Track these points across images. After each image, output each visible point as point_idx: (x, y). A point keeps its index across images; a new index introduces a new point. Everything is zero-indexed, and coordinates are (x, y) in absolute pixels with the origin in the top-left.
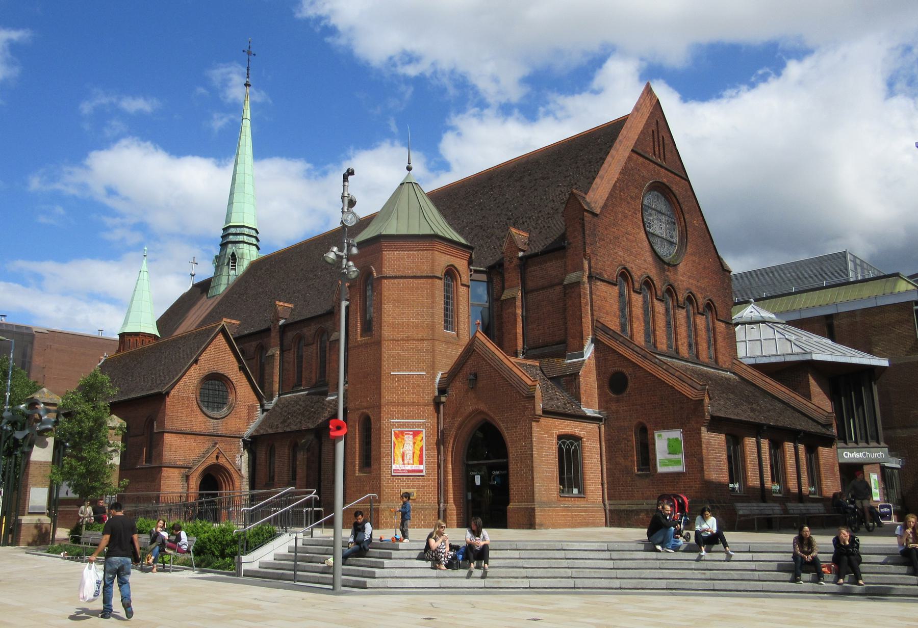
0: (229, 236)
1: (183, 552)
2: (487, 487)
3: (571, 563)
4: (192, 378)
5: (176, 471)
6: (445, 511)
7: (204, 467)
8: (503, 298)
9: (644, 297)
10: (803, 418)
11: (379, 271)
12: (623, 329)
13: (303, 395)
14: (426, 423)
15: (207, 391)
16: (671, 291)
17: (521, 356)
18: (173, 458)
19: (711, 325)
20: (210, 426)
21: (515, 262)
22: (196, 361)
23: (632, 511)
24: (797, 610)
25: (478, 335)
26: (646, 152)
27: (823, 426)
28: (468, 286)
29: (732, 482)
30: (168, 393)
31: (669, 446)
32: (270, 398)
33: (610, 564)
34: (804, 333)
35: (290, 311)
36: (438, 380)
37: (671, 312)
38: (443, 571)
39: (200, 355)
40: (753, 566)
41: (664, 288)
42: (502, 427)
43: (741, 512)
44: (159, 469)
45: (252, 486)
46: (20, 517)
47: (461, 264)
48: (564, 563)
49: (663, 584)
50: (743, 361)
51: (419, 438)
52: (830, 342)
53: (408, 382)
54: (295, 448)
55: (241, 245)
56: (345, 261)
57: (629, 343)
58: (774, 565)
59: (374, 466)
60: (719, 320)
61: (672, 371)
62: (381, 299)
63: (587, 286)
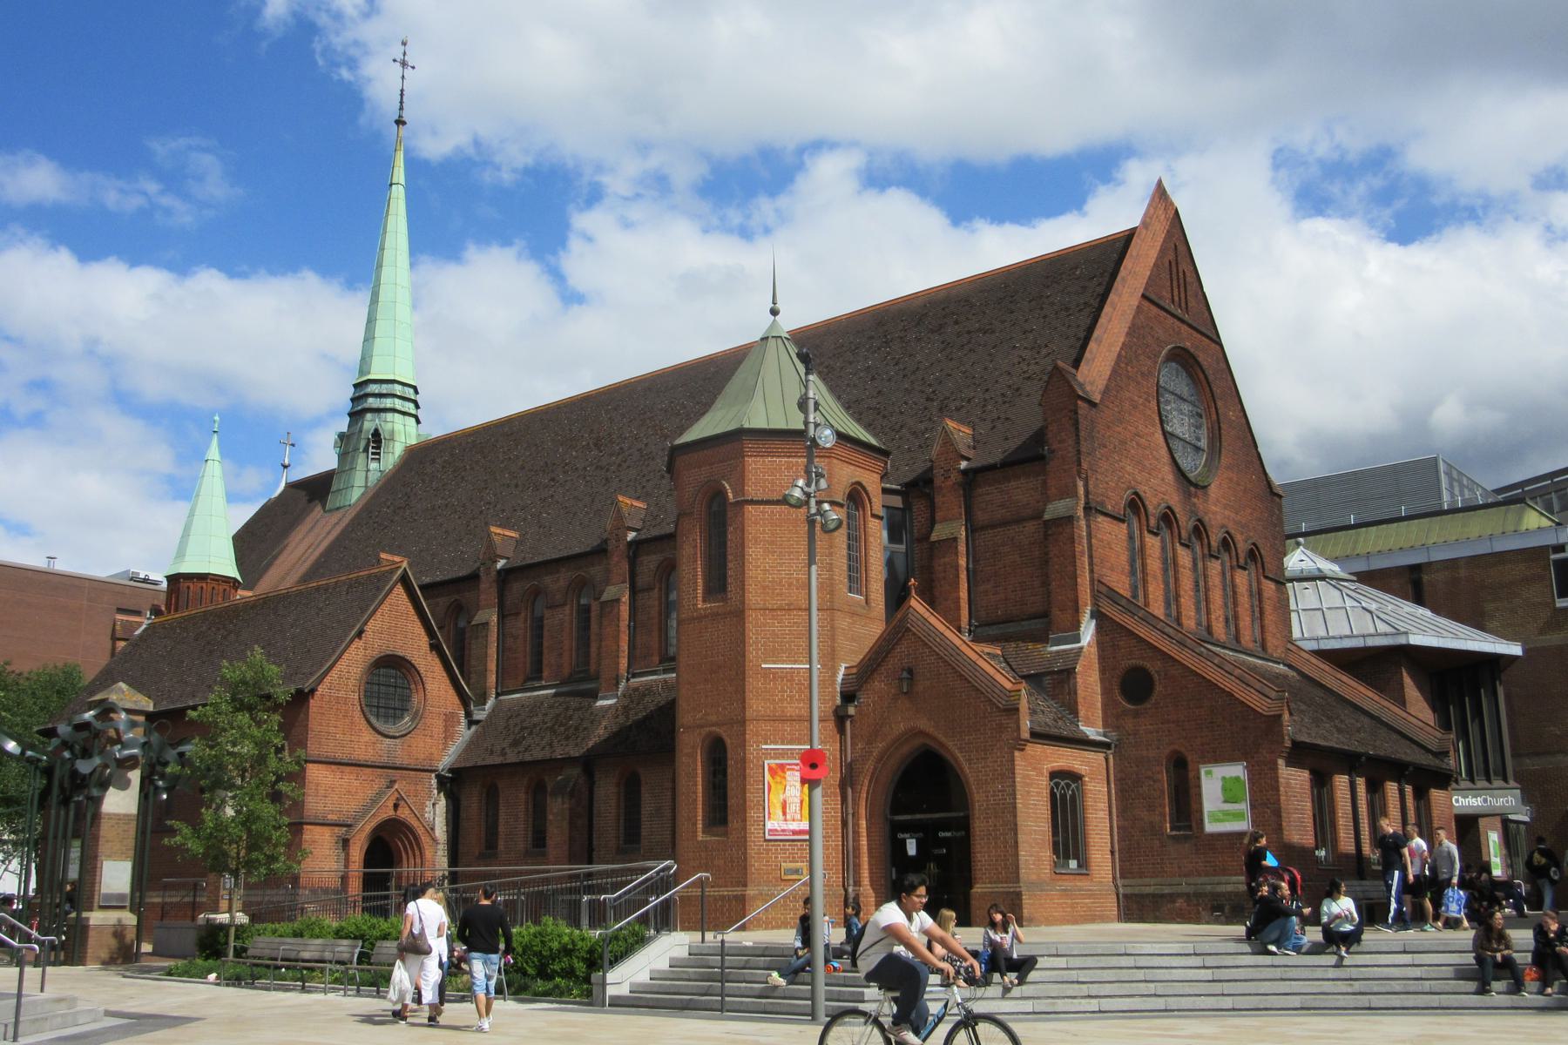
3: (1150, 975)
5: (326, 830)
7: (373, 824)
8: (934, 537)
9: (1163, 541)
11: (740, 487)
15: (376, 688)
16: (1200, 530)
18: (320, 807)
19: (1254, 585)
20: (382, 749)
21: (955, 477)
22: (360, 634)
23: (1162, 896)
26: (1161, 297)
27: (1436, 755)
30: (313, 691)
31: (1224, 789)
32: (482, 700)
34: (1387, 597)
35: (513, 543)
37: (1200, 565)
39: (366, 623)
40: (1417, 972)
41: (1191, 524)
45: (454, 859)
46: (85, 914)
47: (872, 482)
49: (1295, 1001)
53: (792, 680)
54: (538, 792)
55: (389, 416)
57: (1149, 620)
58: (1449, 972)
59: (733, 823)
60: (1266, 577)
61: (1228, 667)
62: (743, 539)
63: (1083, 523)
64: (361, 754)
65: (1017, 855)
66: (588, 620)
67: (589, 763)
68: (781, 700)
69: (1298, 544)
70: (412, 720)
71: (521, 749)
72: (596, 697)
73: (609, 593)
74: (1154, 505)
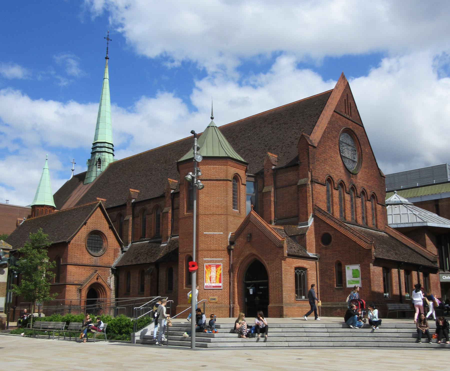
0: (97, 148)
1: (100, 331)
2: (256, 296)
3: (308, 334)
4: (82, 234)
6: (233, 308)
7: (90, 284)
8: (264, 191)
9: (340, 192)
10: (422, 258)
12: (329, 210)
13: (146, 243)
14: (223, 261)
16: (354, 188)
17: (273, 224)
18: (72, 279)
19: (374, 206)
21: (270, 171)
22: (85, 224)
23: (333, 308)
24: (419, 354)
25: (252, 212)
26: (341, 112)
27: (433, 262)
28: (245, 185)
29: (385, 292)
30: (69, 242)
31: (353, 273)
32: (127, 244)
33: (327, 334)
36: (229, 237)
37: (354, 200)
38: (245, 338)
39: (87, 220)
40: (397, 335)
41: (350, 187)
42: (265, 263)
43: (390, 309)
44: (64, 285)
47: (242, 173)
48: (305, 334)
49: (354, 344)
50: (390, 226)
51: (219, 269)
52: (437, 215)
54: (142, 274)
55: (104, 154)
56: (195, 180)
57: (332, 217)
58: (411, 335)
61: (355, 233)
63: (310, 186)
64: (86, 262)
65: (282, 294)
66: (159, 218)
67: (157, 264)
68: (210, 244)
69: (395, 193)
70: (103, 251)
71: (137, 260)
72: (161, 243)
73: (165, 210)
74: (336, 180)
